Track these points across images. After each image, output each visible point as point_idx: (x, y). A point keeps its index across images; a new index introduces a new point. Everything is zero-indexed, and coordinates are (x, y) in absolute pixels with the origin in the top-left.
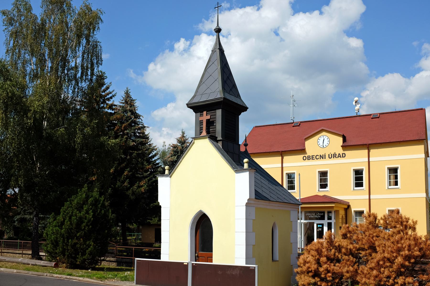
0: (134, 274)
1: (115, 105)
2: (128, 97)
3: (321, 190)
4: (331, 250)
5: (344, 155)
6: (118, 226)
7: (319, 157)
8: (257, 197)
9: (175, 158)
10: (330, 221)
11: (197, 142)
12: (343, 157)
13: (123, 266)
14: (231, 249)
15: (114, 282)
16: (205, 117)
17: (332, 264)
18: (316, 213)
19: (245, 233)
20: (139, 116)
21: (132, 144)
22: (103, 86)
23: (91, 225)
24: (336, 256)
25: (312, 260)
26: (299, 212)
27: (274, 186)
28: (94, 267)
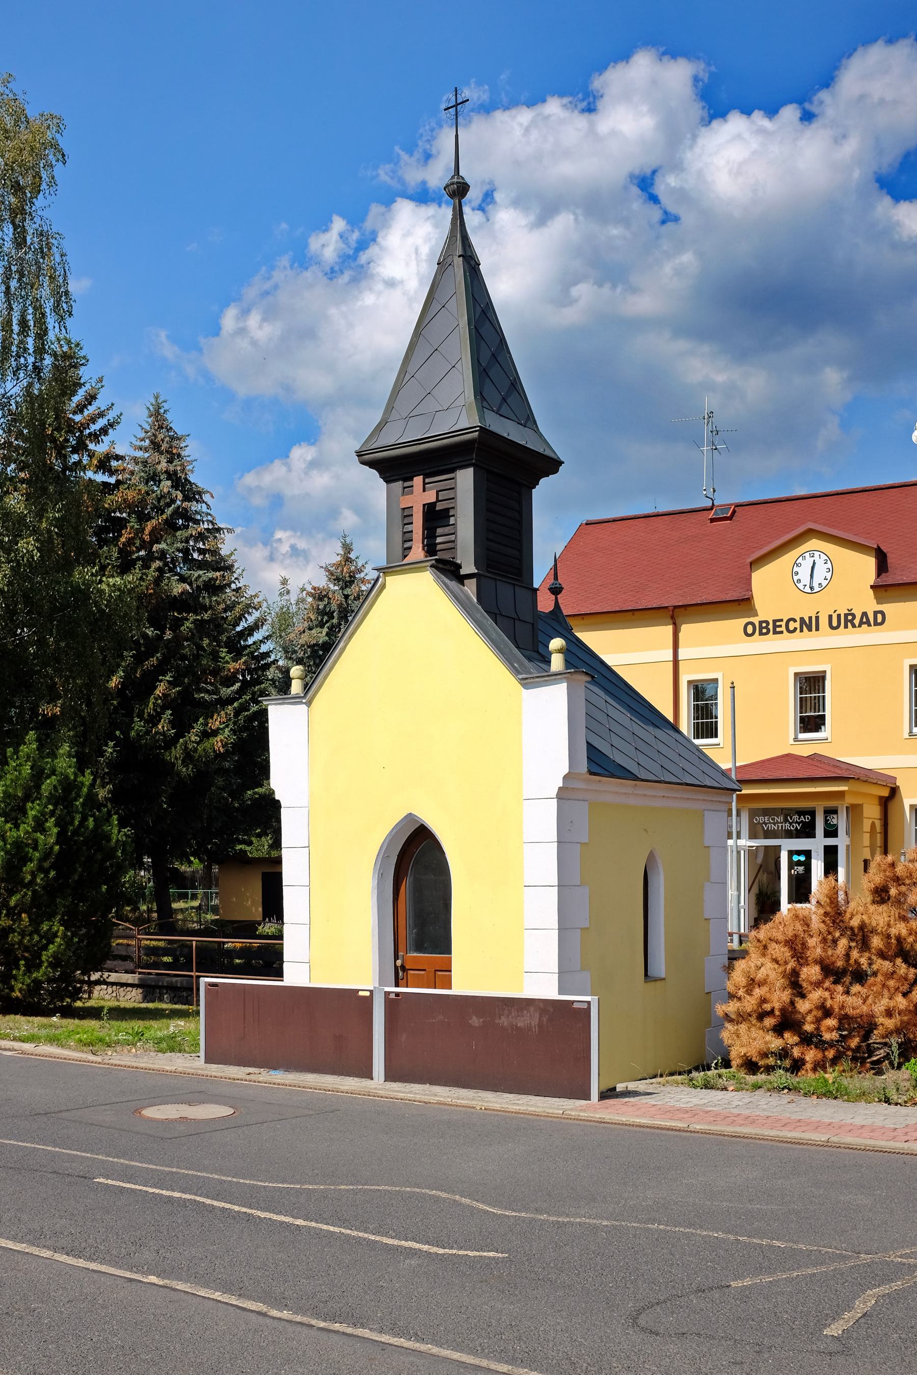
0: (198, 1029)
1: (118, 458)
2: (161, 427)
3: (802, 736)
4: (835, 941)
5: (879, 617)
6: (141, 865)
7: (797, 625)
8: (596, 769)
9: (321, 635)
10: (831, 842)
11: (393, 582)
12: (876, 624)
13: (161, 1000)
14: (510, 942)
15: (136, 1056)
16: (421, 494)
17: (840, 988)
18: (787, 813)
20: (200, 493)
21: (178, 588)
22: (74, 393)
23: (53, 866)
24: (852, 961)
25: (773, 976)
26: (730, 815)
27: (650, 729)
28: (69, 1006)
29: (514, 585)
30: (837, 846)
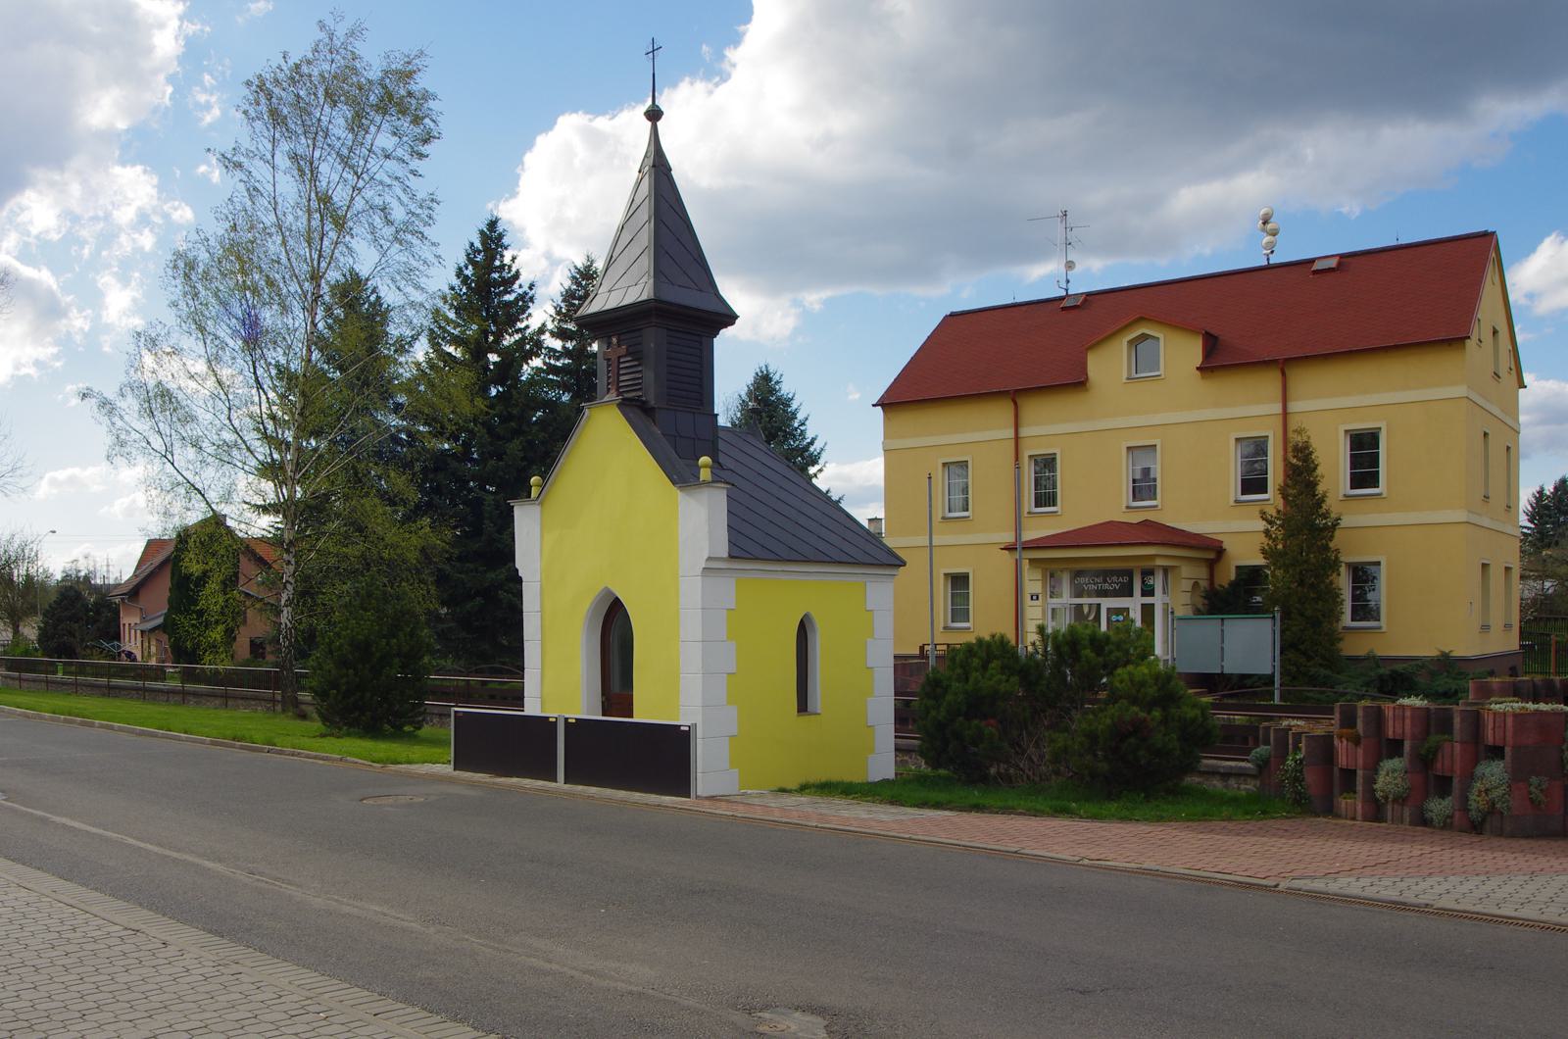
10: (1148, 600)
18: (1106, 574)
19: (525, 638)
29: (694, 413)
30: (1153, 604)
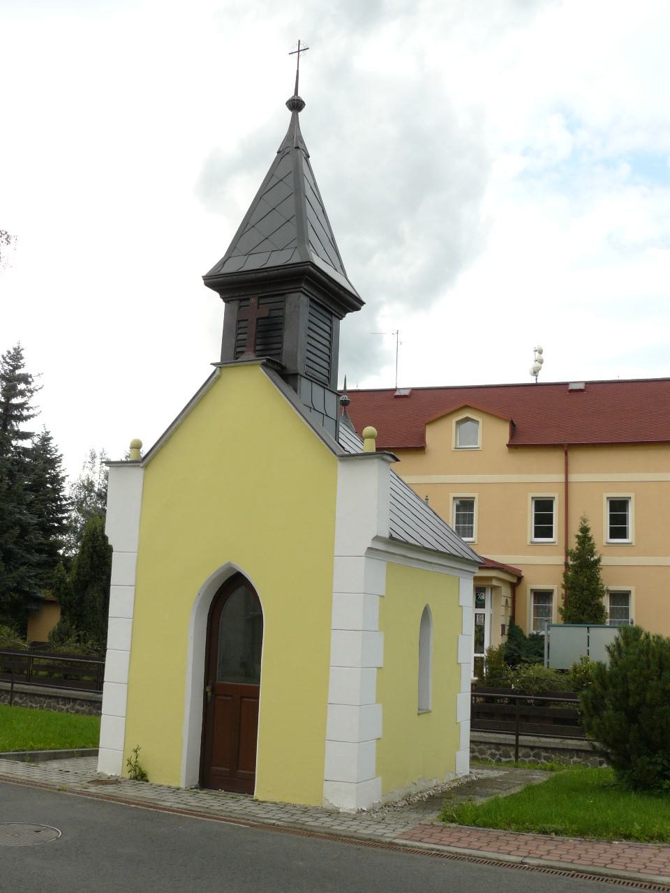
10: (480, 611)
